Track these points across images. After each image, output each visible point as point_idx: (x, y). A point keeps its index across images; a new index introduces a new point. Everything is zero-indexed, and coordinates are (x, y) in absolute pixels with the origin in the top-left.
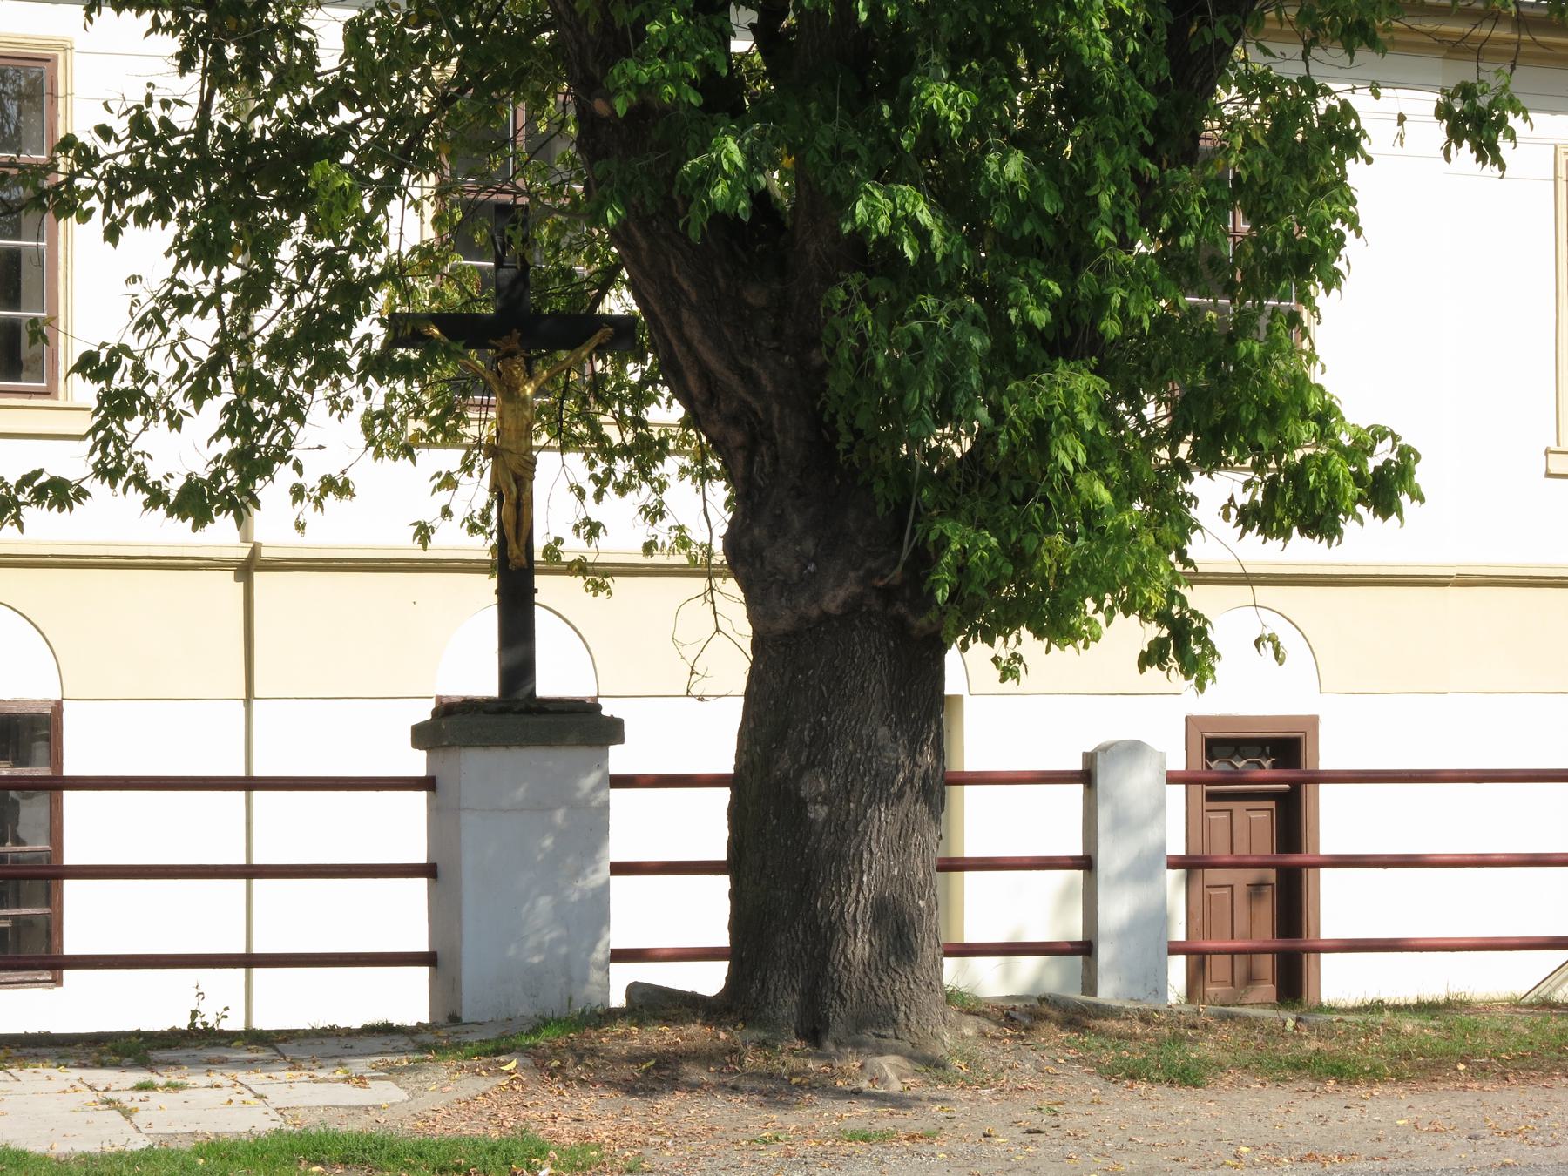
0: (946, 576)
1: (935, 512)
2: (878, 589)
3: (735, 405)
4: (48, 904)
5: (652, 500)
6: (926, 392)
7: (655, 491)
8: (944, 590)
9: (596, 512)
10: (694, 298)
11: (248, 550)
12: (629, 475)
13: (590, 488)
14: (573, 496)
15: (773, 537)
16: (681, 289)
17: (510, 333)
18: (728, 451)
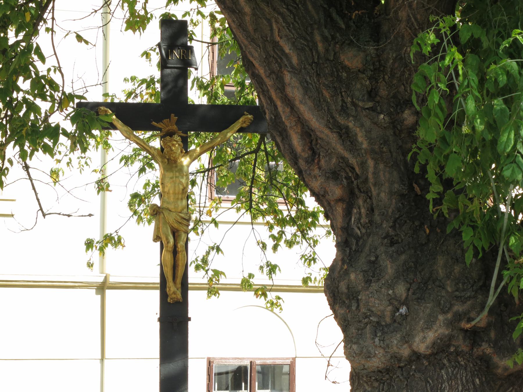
2: (466, 331)
3: (334, 160)
5: (308, 251)
7: (310, 245)
9: (273, 258)
10: (295, 60)
12: (295, 235)
13: (270, 243)
14: (258, 249)
15: (368, 282)
16: (283, 51)
17: (169, 117)
18: (329, 204)
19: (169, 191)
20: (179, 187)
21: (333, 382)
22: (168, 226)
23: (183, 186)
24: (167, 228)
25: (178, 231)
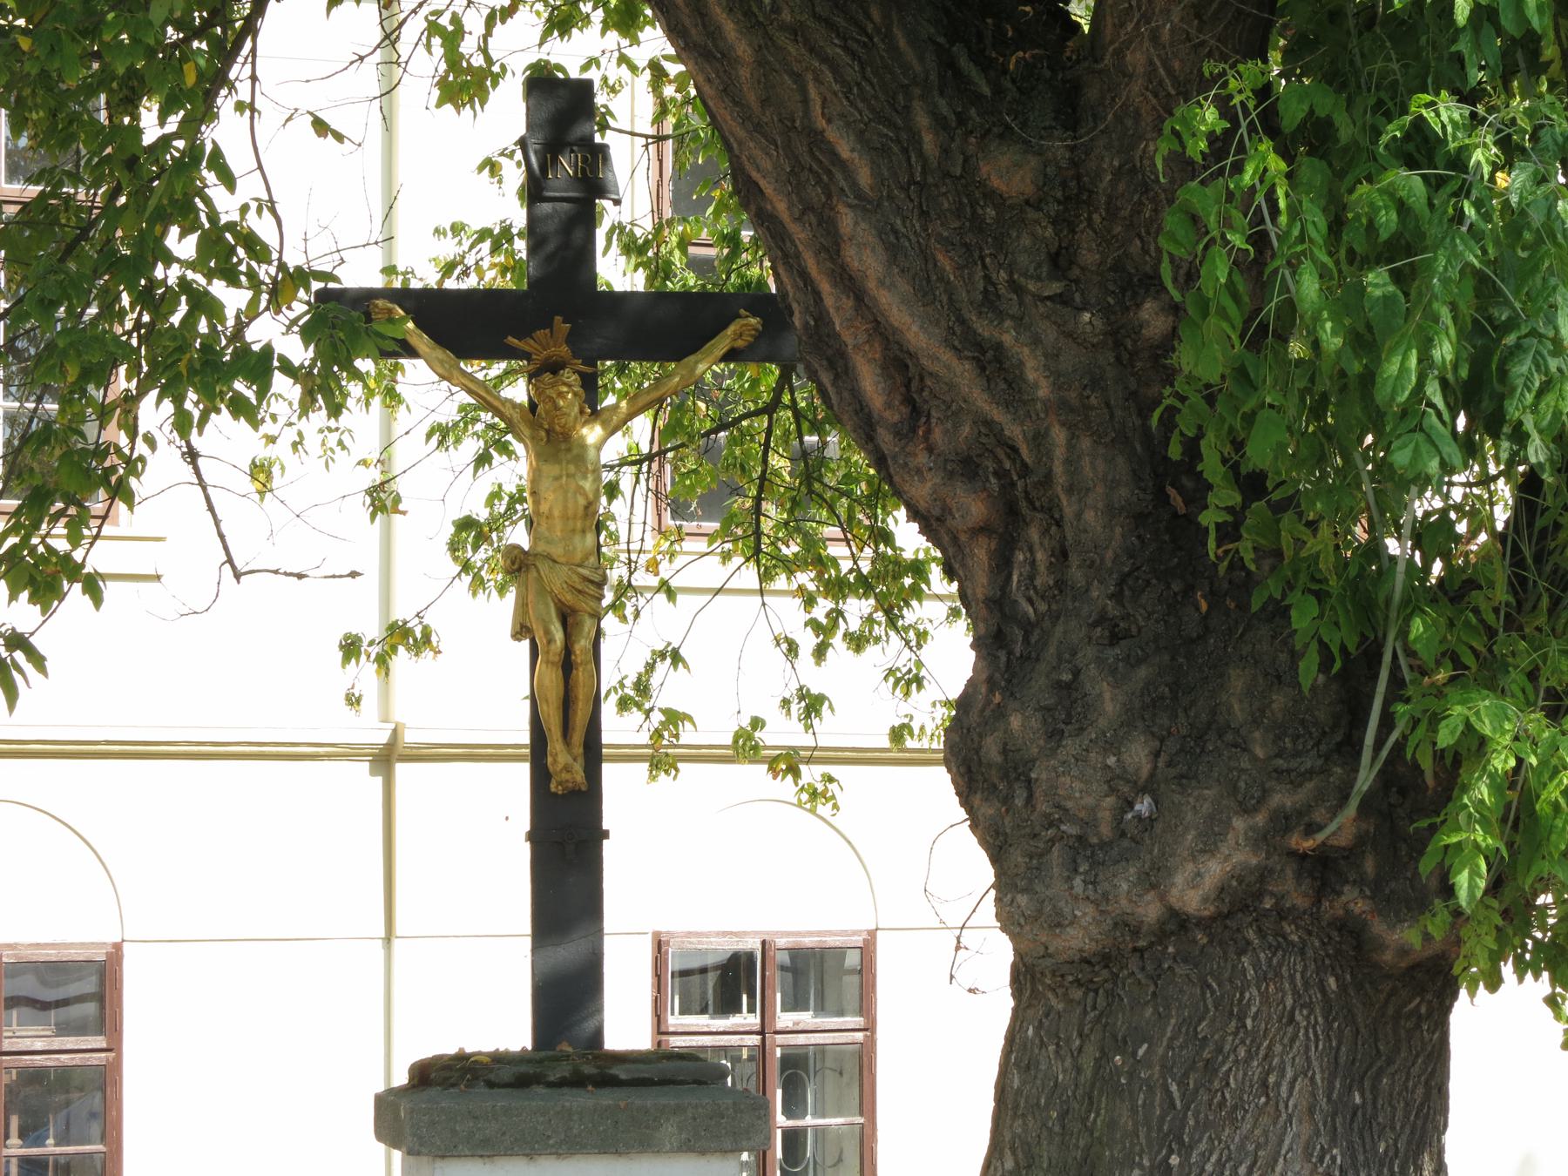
0: (1479, 835)
1: (1442, 676)
3: (966, 430)
5: (904, 660)
6: (1437, 354)
7: (907, 643)
8: (1475, 873)
10: (864, 177)
11: (389, 732)
12: (869, 620)
14: (778, 655)
17: (549, 324)
19: (550, 509)
21: (970, 991)
23: (586, 497)
24: (547, 605)
25: (574, 611)
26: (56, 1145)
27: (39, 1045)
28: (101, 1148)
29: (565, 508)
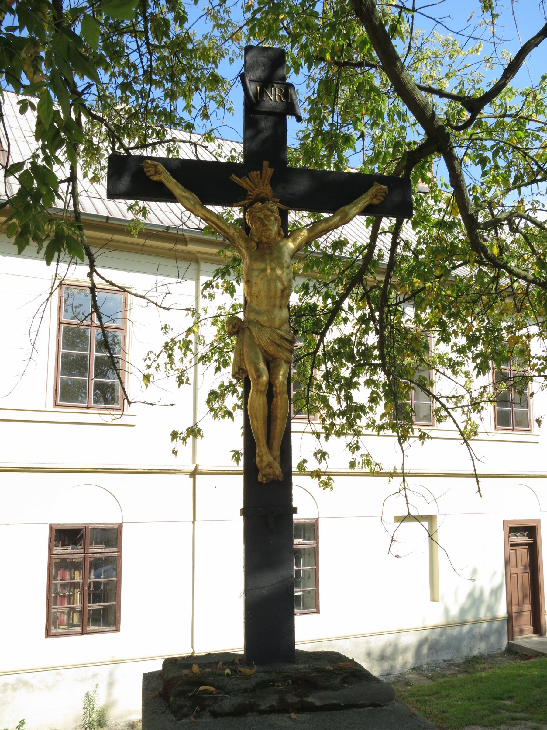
4: (115, 601)
19: (259, 292)
20: (276, 286)
21: (396, 556)
22: (258, 350)
23: (283, 284)
24: (256, 353)
25: (274, 358)
26: (104, 578)
27: (99, 551)
28: (115, 579)
29: (269, 290)
